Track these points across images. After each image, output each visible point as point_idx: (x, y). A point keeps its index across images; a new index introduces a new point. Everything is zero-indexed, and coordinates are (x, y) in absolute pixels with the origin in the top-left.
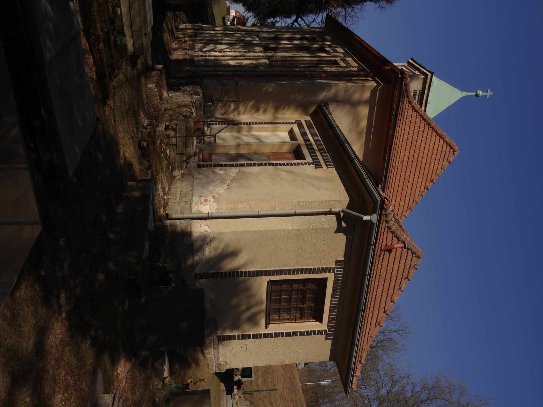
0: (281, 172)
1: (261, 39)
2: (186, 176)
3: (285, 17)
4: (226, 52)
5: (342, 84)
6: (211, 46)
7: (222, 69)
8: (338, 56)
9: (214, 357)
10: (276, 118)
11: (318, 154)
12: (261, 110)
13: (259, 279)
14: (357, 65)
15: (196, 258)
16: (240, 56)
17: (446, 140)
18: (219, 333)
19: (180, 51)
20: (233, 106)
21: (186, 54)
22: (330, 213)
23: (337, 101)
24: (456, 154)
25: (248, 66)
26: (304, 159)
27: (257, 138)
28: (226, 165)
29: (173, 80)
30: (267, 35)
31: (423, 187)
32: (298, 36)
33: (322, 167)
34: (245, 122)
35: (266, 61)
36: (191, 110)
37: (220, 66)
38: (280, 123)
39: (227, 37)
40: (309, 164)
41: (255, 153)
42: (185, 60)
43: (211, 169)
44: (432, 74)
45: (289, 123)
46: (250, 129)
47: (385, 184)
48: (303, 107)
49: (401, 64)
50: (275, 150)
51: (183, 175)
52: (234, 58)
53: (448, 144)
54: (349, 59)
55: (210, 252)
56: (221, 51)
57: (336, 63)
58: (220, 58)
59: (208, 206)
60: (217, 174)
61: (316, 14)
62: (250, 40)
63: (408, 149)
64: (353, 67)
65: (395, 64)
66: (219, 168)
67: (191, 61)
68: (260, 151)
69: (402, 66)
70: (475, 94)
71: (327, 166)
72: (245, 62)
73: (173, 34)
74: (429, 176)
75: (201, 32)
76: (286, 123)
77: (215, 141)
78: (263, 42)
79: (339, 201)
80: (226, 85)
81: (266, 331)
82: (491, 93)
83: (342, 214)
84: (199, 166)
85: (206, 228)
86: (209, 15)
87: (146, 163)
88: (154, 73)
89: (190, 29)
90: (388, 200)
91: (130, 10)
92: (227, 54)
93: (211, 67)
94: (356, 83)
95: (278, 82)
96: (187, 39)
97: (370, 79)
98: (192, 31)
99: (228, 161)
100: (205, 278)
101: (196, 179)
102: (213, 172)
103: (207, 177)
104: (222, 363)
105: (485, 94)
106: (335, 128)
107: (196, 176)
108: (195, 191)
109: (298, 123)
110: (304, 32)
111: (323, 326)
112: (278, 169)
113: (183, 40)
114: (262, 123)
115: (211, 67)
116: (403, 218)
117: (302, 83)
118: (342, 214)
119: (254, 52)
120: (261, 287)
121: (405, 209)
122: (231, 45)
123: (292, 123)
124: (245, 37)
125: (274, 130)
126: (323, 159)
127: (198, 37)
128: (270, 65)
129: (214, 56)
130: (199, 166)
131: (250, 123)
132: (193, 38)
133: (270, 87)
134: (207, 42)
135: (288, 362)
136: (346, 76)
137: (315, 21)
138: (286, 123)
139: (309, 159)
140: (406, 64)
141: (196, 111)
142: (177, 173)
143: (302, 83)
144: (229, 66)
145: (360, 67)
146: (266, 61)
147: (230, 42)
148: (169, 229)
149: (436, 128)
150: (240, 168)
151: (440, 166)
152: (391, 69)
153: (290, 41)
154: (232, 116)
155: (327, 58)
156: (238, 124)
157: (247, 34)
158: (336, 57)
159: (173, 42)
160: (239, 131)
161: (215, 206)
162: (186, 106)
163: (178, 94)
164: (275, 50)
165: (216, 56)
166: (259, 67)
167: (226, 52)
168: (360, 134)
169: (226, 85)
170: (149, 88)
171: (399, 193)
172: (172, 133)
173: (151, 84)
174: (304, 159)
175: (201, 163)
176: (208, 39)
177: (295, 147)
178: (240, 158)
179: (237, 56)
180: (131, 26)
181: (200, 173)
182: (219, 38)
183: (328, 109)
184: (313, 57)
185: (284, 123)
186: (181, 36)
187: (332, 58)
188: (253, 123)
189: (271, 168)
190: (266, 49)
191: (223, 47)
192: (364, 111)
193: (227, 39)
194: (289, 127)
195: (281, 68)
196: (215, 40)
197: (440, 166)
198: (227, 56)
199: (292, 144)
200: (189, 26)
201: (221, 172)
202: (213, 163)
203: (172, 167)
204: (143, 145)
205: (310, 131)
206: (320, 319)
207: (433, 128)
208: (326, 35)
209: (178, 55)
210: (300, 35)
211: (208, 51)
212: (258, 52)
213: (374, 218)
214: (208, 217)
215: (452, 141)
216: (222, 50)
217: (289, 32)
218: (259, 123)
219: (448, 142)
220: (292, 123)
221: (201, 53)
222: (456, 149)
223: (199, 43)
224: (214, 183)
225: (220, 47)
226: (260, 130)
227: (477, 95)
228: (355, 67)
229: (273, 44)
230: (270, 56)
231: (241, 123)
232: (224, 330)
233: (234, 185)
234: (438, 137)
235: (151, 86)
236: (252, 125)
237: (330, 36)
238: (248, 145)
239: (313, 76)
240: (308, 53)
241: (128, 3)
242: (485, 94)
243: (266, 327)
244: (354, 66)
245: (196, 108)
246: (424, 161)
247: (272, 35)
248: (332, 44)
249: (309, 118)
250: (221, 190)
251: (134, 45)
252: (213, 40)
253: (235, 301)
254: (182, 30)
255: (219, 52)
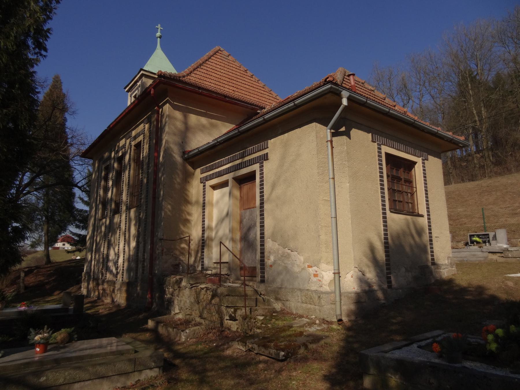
0: (274, 195)
1: (103, 216)
2: (279, 296)
3: (74, 198)
4: (118, 250)
5: (165, 137)
6: (111, 264)
7: (140, 255)
8: (130, 143)
9: (447, 269)
10: (197, 202)
11: (247, 159)
12: (188, 217)
13: (389, 222)
14: (142, 125)
15: (375, 287)
16: (125, 236)
17: (212, 54)
18: (430, 264)
19: (116, 295)
20: (183, 245)
21: (120, 289)
22: (331, 142)
23: (183, 142)
24: (222, 49)
25: (139, 228)
26: (254, 172)
27: (221, 221)
28: (262, 253)
29: (154, 306)
30: (100, 211)
31: (252, 79)
32: (103, 183)
33: (267, 154)
34: (201, 232)
35: (133, 211)
36: (202, 289)
37: (137, 256)
38: (204, 197)
39: (100, 248)
40: (262, 167)
41: (241, 222)
42: (127, 291)
43: (267, 269)
44: (142, 70)
45: (204, 189)
46: (210, 228)
47: (257, 106)
48: (187, 177)
49: (129, 97)
50: (238, 203)
51: (277, 299)
52: (127, 242)
53: (215, 54)
54: (134, 133)
55: (370, 272)
56: (117, 255)
57: (138, 146)
58: (126, 256)
59: (324, 273)
60: (275, 262)
61: (73, 171)
62: (106, 227)
63: (224, 85)
64: (145, 128)
65: (129, 104)
66: (266, 260)
67: (130, 285)
68: (239, 218)
69: (131, 96)
70: (159, 39)
71: (265, 149)
72: (133, 231)
73: (95, 302)
74: (242, 72)
75: (92, 274)
76: (204, 192)
77: (227, 263)
78: (109, 214)
79: (317, 133)
80: (163, 250)
81: (426, 217)
82: (159, 25)
83: (332, 131)
84: (263, 281)
85: (349, 276)
86: (69, 265)
87: (302, 351)
88: (161, 330)
89: (88, 284)
90: (328, 78)
91: (106, 377)
92: (122, 250)
93: (137, 265)
94: (166, 123)
95: (161, 199)
96: (100, 287)
97: (161, 110)
98: (91, 282)
99: (256, 250)
100: (390, 278)
101: (282, 285)
102: (271, 266)
103: (279, 273)
104: (449, 261)
105: (159, 30)
106: (218, 142)
107: (277, 284)
108: (301, 287)
109: (203, 181)
110: (98, 177)
111: (419, 160)
112: (268, 199)
113: (101, 292)
114: (204, 215)
115: (137, 265)
116: (278, 97)
117: (163, 175)
118: (332, 131)
119: (120, 223)
120: (397, 221)
121: (270, 95)
122: (110, 245)
123: (204, 186)
124: (101, 232)
125: (212, 204)
126: (254, 153)
127: (98, 277)
128: (138, 207)
129: (124, 262)
130: (263, 281)
131: (203, 228)
132: (100, 282)
133: (167, 207)
134: (105, 268)
135: (444, 198)
136: (157, 134)
137: (81, 170)
138: (204, 192)
139: (256, 167)
140: (129, 93)
141: (201, 283)
142: (278, 306)
143: (163, 175)
144: (137, 247)
145: (145, 121)
146: (133, 211)
147: (106, 246)
148: (353, 318)
149: (203, 60)
150: (265, 238)
151: (232, 63)
152: (154, 88)
153: (109, 190)
154: (193, 245)
155: (132, 153)
156: (203, 240)
157: (97, 230)
158: (131, 146)
159: (103, 301)
160: (211, 239)
161: (323, 266)
162: (198, 294)
163: (176, 302)
164: (118, 205)
165: (124, 259)
166: (140, 218)
167: (118, 250)
168: (213, 126)
169: (163, 250)
170: (186, 339)
171: (260, 98)
172: (239, 312)
173: (180, 337)
174: (254, 172)
175: (259, 279)
176: (101, 267)
177: (234, 182)
178: (250, 238)
179: (125, 239)
180: (126, 374)
181: (274, 281)
182: (101, 256)
183: (191, 151)
184: (130, 166)
185: (204, 194)
186: (97, 293)
187: (132, 149)
188: (203, 224)
189: (266, 206)
190: (117, 211)
191: (112, 253)
192: (193, 119)
193: (103, 249)
194: (208, 189)
195: (143, 196)
196: (103, 260)
197: (232, 63)
198: (124, 249)
199: (233, 186)
200: (84, 285)
201: (272, 258)
202: (259, 266)
203: (272, 314)
204: (284, 356)
205: (216, 168)
206: (415, 163)
207: (203, 63)
208: (103, 157)
209: (121, 298)
210: (101, 181)
211: (117, 269)
212: (121, 219)
213: (345, 94)
214: (337, 273)
215: (212, 50)
216: (115, 254)
217: (97, 191)
218: (204, 218)
219: (213, 53)
220: (204, 186)
221: (120, 276)
222: (218, 48)
223: (106, 276)
224: (289, 267)
225: (112, 256)
226: (211, 219)
227: (160, 37)
228: (144, 126)
229: (111, 205)
230: (127, 207)
231: (203, 237)
232: (427, 260)
233: (292, 245)
234: (210, 60)
235: (183, 337)
236: (206, 226)
237: (105, 154)
238: (232, 230)
239: (156, 165)
240: (124, 172)
241: (98, 380)
242: (159, 30)
243: (422, 216)
244: (143, 127)
245: (198, 283)
246: (231, 74)
247: (100, 206)
248: (114, 150)
249: (198, 170)
250: (299, 260)
251: (151, 369)
252: (103, 263)
253: (408, 249)
254: (88, 291)
255: (118, 257)
